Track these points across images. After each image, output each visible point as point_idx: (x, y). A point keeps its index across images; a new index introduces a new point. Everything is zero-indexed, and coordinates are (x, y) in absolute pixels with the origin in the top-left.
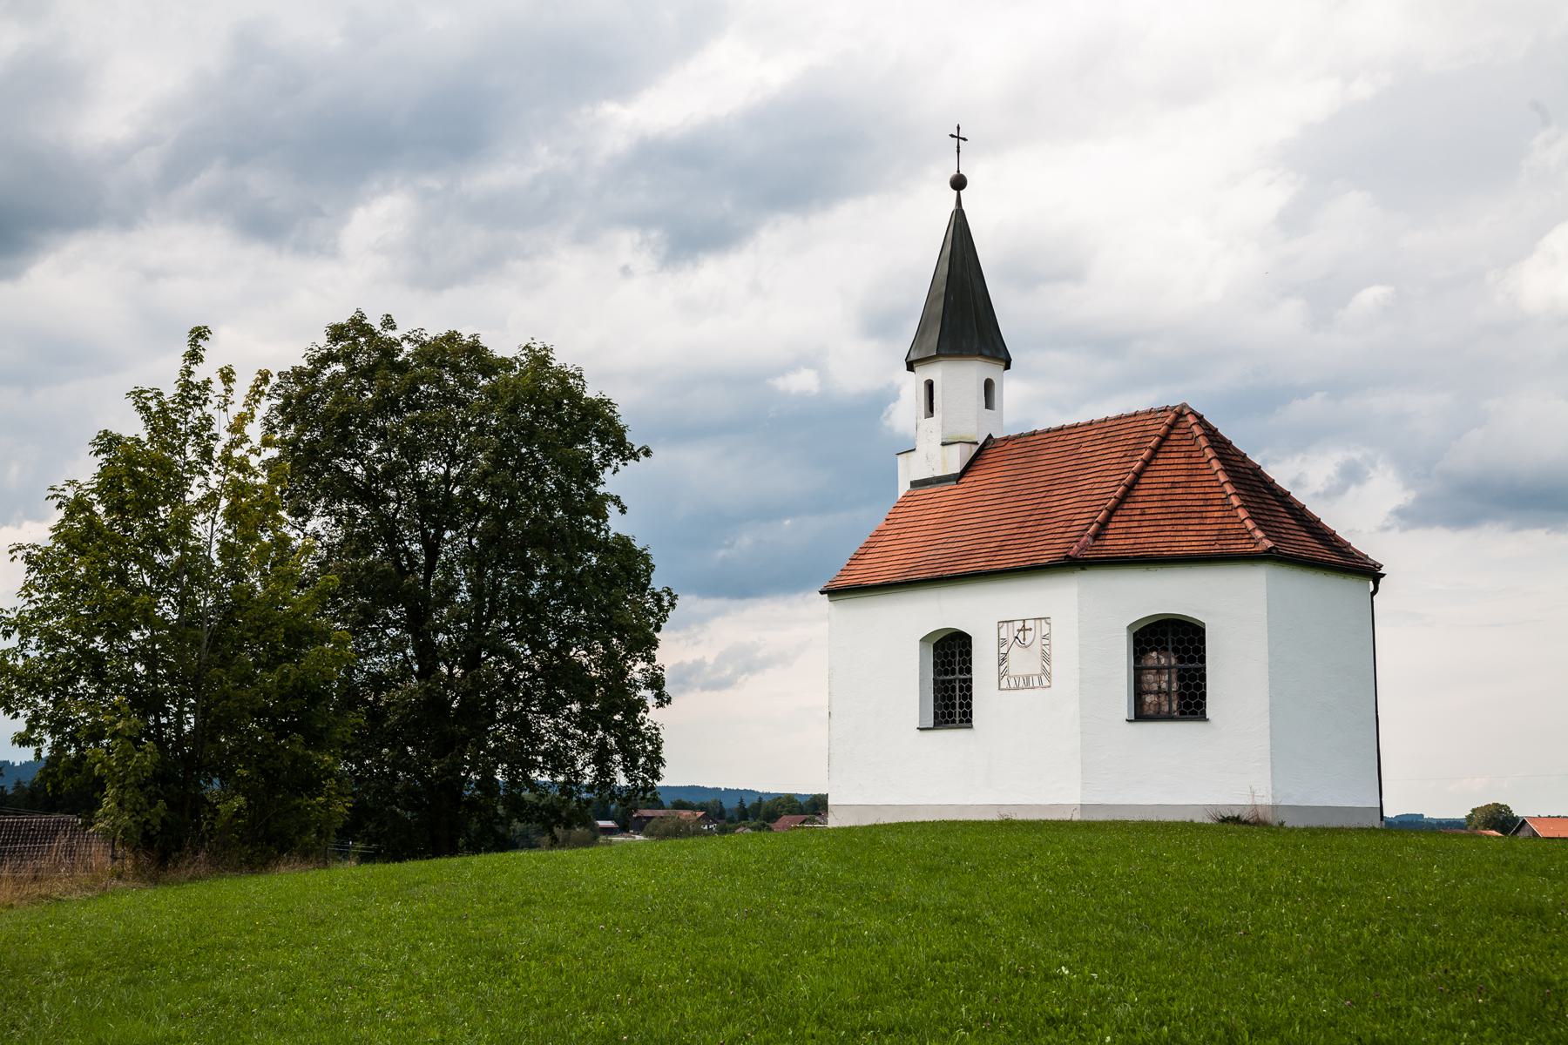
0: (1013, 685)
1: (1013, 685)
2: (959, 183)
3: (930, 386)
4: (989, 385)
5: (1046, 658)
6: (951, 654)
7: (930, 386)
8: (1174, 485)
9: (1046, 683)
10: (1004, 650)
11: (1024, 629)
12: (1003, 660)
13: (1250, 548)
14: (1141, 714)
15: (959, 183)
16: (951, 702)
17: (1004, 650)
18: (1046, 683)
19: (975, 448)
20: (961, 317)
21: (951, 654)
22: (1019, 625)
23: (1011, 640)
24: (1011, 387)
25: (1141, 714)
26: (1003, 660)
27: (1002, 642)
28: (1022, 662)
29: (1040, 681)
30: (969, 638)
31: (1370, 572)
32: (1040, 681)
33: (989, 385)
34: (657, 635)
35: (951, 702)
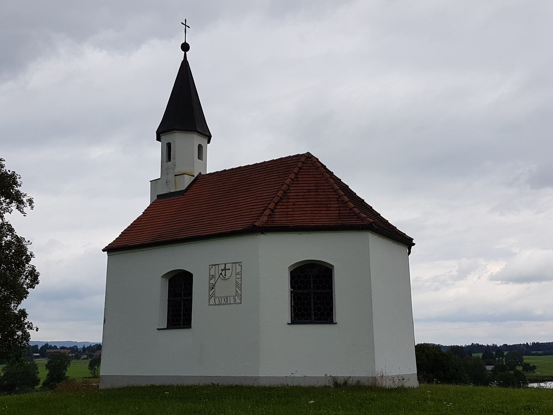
0: (217, 302)
1: (217, 302)
2: (185, 47)
3: (169, 145)
4: (200, 147)
5: (239, 286)
6: (180, 286)
7: (169, 145)
8: (309, 190)
9: (238, 301)
10: (212, 281)
11: (225, 269)
12: (212, 287)
13: (359, 222)
14: (190, 327)
15: (185, 47)
16: (179, 313)
17: (212, 281)
18: (238, 301)
19: (193, 178)
20: (184, 113)
21: (180, 286)
22: (222, 267)
23: (217, 277)
24: (211, 149)
25: (190, 327)
26: (212, 287)
27: (212, 277)
28: (224, 289)
29: (235, 299)
30: (191, 275)
31: (407, 242)
32: (235, 299)
33: (200, 147)
34: (29, 290)
35: (179, 313)
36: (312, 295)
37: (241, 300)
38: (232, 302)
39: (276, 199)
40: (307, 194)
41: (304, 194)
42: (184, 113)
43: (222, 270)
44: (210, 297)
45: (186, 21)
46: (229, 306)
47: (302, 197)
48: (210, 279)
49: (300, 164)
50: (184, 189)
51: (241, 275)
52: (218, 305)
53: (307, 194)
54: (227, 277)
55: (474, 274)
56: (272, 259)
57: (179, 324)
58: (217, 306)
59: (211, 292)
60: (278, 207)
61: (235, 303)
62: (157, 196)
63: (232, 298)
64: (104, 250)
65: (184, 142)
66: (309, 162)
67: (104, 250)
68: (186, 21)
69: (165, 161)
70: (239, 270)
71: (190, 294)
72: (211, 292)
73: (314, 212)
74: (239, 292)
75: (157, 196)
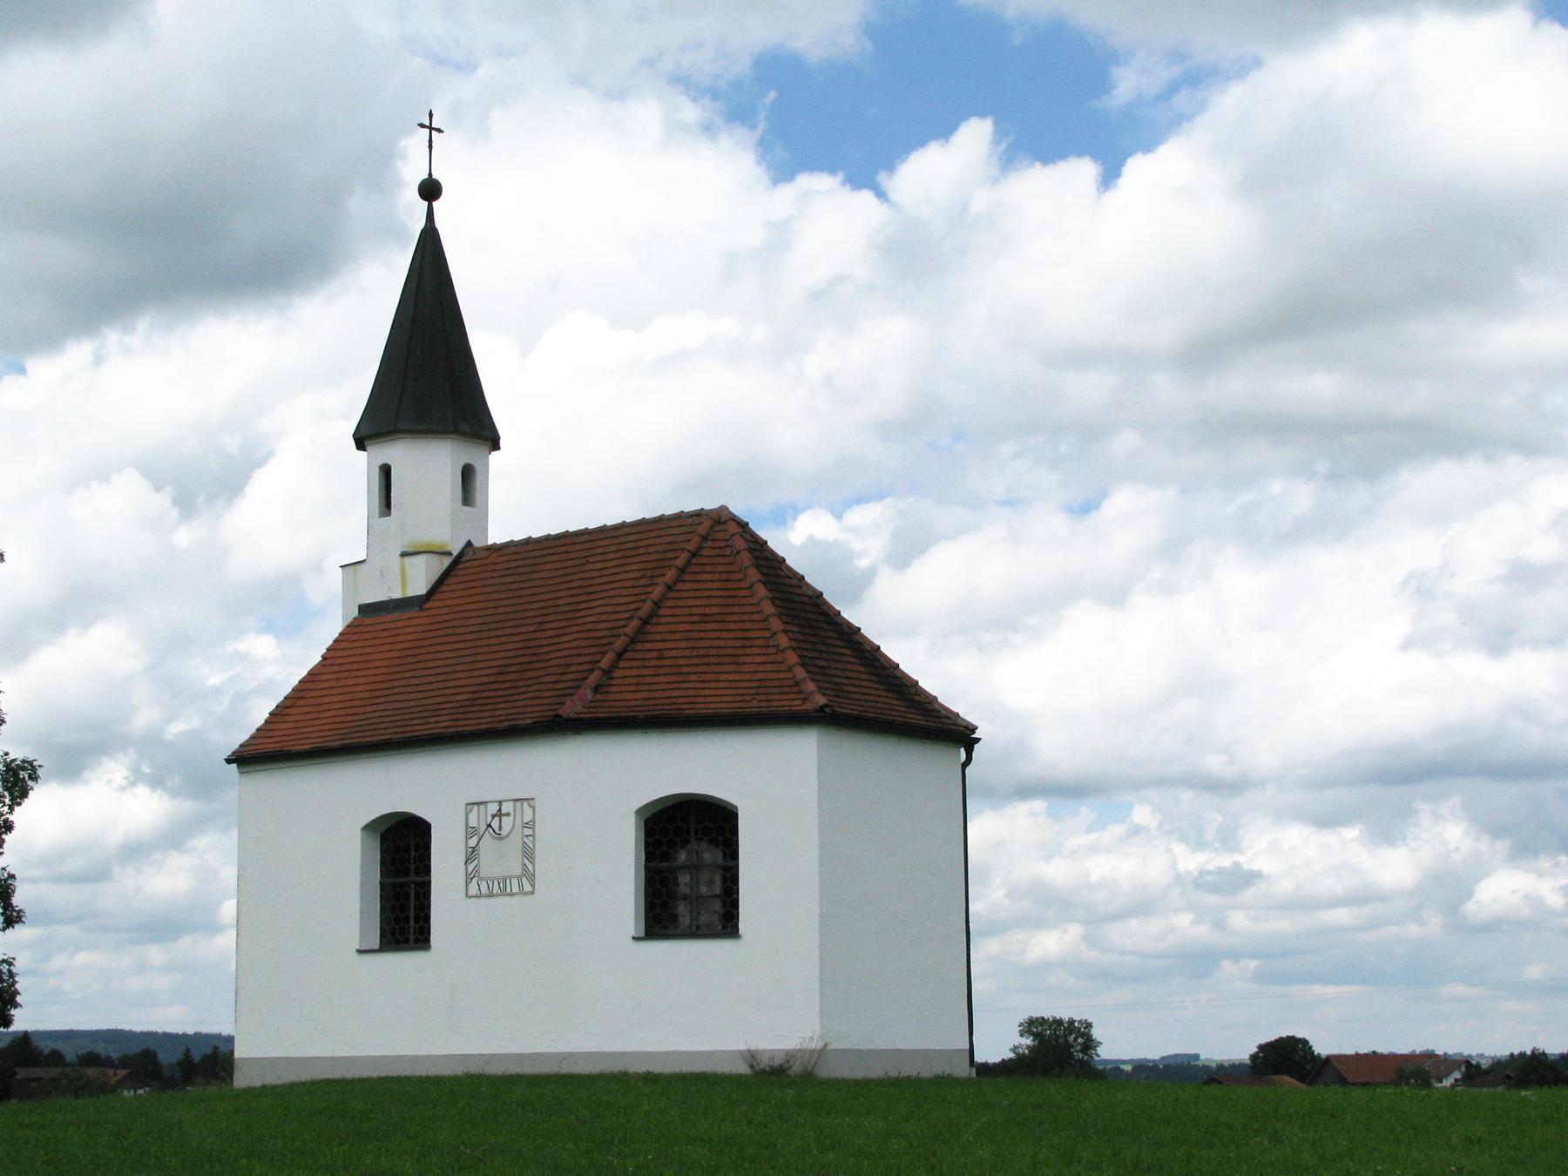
0: (484, 890)
1: (484, 890)
2: (430, 190)
3: (386, 471)
4: (468, 474)
5: (528, 853)
6: (402, 846)
7: (386, 471)
9: (527, 888)
10: (473, 842)
11: (499, 814)
15: (430, 190)
16: (403, 918)
17: (473, 842)
18: (527, 888)
19: (447, 561)
20: (428, 383)
21: (402, 846)
22: (493, 808)
27: (470, 832)
28: (499, 860)
33: (468, 474)
35: (403, 918)
36: (689, 868)
37: (533, 886)
38: (516, 889)
39: (619, 643)
40: (697, 627)
41: (689, 627)
42: (428, 383)
43: (493, 816)
44: (469, 878)
45: (431, 115)
46: (508, 899)
47: (684, 635)
48: (468, 837)
49: (702, 530)
50: (423, 592)
51: (533, 828)
52: (486, 896)
53: (697, 627)
54: (504, 832)
55: (1193, 753)
56: (589, 795)
57: (406, 941)
58: (483, 900)
59: (471, 868)
60: (622, 664)
61: (523, 893)
62: (360, 607)
63: (515, 882)
64: (228, 761)
65: (426, 464)
66: (720, 536)
67: (228, 761)
68: (431, 115)
69: (377, 513)
70: (528, 818)
71: (427, 870)
72: (471, 868)
73: (703, 677)
74: (530, 867)
75: (360, 607)
